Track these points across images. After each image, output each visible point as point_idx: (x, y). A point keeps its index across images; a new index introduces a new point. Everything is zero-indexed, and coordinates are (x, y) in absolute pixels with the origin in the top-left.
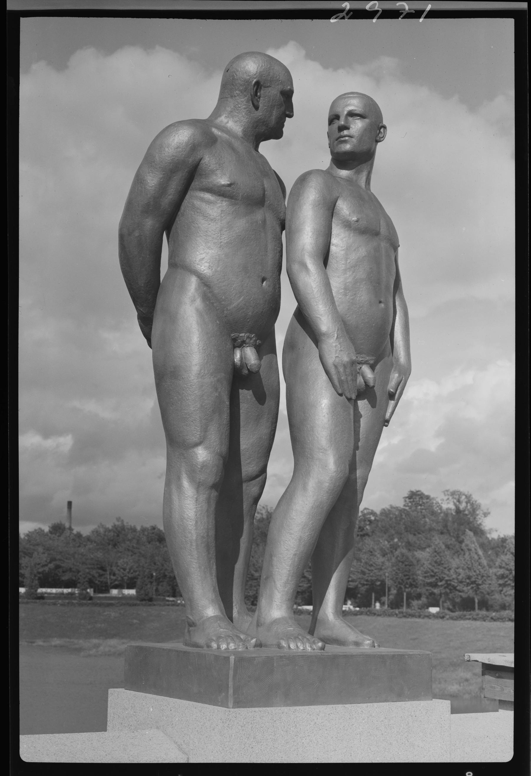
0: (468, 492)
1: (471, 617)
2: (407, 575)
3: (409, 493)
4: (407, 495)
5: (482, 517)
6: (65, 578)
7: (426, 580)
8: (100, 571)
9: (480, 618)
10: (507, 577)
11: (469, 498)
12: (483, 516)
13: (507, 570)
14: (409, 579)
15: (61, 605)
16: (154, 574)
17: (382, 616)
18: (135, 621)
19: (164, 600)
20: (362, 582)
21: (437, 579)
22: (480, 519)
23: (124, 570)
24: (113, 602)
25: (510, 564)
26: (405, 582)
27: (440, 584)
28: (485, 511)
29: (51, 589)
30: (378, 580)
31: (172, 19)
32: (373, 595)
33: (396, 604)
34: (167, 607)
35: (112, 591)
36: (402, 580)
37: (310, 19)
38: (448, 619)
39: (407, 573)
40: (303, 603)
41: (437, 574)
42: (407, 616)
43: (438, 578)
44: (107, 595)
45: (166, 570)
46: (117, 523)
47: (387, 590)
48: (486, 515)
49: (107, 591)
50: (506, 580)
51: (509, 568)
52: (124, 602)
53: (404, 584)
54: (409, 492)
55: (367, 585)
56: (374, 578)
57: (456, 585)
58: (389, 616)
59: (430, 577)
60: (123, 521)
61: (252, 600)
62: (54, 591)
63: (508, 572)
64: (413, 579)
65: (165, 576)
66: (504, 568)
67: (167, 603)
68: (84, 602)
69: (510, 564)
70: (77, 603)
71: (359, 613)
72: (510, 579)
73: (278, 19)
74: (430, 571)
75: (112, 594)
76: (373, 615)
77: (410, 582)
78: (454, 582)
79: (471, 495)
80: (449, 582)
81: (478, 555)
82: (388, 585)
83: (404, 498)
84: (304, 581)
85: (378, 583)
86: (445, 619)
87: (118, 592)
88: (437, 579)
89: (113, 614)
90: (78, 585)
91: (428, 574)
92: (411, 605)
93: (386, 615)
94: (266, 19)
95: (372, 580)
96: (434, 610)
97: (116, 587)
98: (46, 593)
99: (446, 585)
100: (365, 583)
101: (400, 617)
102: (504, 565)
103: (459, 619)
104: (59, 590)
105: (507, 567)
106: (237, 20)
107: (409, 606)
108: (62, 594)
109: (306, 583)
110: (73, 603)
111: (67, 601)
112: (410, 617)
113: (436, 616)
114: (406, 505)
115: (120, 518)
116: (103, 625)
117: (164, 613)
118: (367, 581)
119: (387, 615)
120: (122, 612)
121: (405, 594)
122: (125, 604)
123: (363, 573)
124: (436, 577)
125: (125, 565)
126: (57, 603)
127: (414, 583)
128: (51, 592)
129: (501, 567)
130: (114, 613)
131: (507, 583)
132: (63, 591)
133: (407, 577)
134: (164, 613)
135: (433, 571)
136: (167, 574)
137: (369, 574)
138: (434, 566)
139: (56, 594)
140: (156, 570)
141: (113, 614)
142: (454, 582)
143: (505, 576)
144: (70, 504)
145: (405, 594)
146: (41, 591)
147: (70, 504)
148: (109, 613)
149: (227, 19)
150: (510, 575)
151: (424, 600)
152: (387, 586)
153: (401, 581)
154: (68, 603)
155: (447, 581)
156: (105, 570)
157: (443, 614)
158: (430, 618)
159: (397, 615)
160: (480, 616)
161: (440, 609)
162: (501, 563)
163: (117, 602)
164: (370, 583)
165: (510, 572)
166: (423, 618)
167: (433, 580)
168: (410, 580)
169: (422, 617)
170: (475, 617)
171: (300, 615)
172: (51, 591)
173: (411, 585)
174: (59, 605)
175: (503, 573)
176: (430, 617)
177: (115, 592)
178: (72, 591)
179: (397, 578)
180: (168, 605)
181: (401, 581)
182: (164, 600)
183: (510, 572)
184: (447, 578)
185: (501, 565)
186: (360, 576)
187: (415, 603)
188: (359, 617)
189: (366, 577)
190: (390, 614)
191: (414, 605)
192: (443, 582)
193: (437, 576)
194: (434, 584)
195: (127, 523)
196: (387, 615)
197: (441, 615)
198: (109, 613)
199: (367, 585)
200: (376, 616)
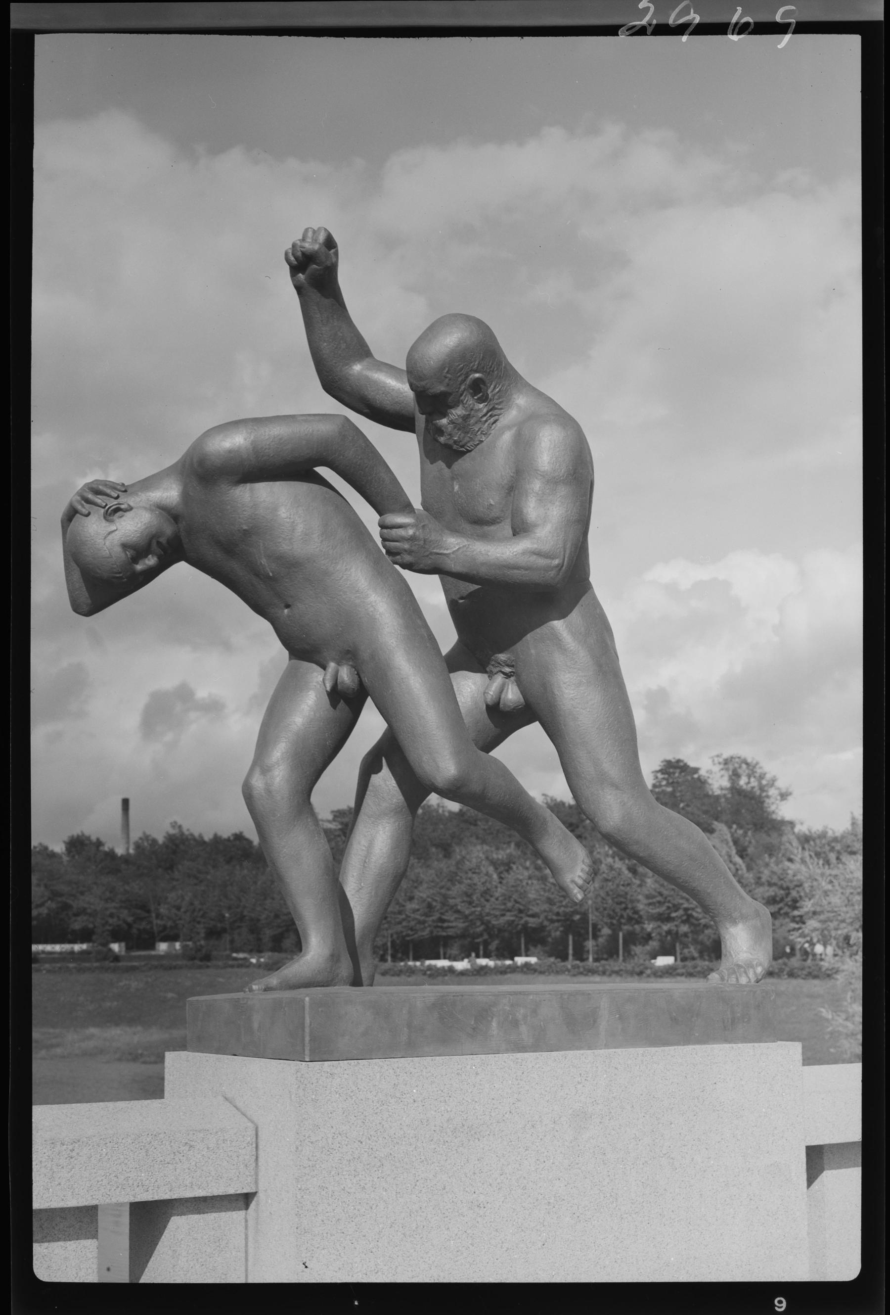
0: (753, 758)
1: (683, 971)
2: (621, 903)
3: (662, 764)
4: (658, 768)
5: (777, 800)
6: (77, 925)
7: (650, 911)
8: (139, 911)
9: (699, 972)
10: (782, 900)
11: (752, 768)
12: (779, 798)
13: (781, 888)
14: (625, 909)
15: (49, 971)
16: (227, 915)
17: (547, 974)
18: (170, 995)
19: (229, 957)
20: (549, 917)
21: (668, 908)
22: (773, 803)
23: (178, 908)
24: (135, 964)
25: (785, 878)
26: (619, 914)
27: (674, 915)
28: (784, 791)
29: (53, 946)
30: (576, 912)
31: (277, 37)
32: (571, 938)
33: (610, 952)
34: (229, 970)
35: (159, 946)
36: (614, 911)
37: (518, 36)
38: (649, 976)
39: (622, 900)
40: (463, 955)
41: (669, 898)
42: (585, 973)
43: (670, 905)
44: (153, 953)
45: (245, 907)
46: (172, 831)
47: (590, 929)
48: (784, 796)
49: (152, 947)
50: (781, 905)
51: (785, 886)
52: (155, 963)
53: (617, 918)
54: (662, 762)
55: (558, 921)
56: (569, 910)
57: (700, 916)
58: (558, 973)
59: (657, 905)
60: (180, 827)
61: (381, 952)
62: (57, 948)
63: (782, 892)
64: (633, 908)
65: (242, 918)
66: (775, 884)
67: (231, 963)
68: (87, 965)
69: (785, 878)
70: (75, 968)
71: (508, 970)
72: (787, 905)
73: (465, 37)
74: (656, 894)
75: (159, 950)
76: (532, 972)
77: (628, 915)
78: (697, 912)
79: (757, 763)
80: (690, 912)
81: (735, 864)
82: (592, 920)
83: (653, 772)
84: (460, 919)
85: (577, 917)
86: (644, 975)
87: (169, 947)
88: (668, 908)
89: (134, 984)
90: (94, 937)
91: (654, 900)
92: (633, 953)
93: (553, 971)
94: (445, 37)
95: (565, 914)
96: (664, 961)
97: (164, 940)
98: (43, 952)
99: (685, 918)
100: (555, 918)
101: (574, 975)
102: (775, 880)
103: (667, 975)
104: (67, 947)
105: (780, 883)
106: (396, 39)
107: (628, 954)
108: (72, 952)
109: (462, 921)
110: (68, 967)
111: (59, 965)
112: (590, 974)
113: (668, 972)
114: (658, 784)
115: (175, 822)
116: (115, 1003)
117: (221, 980)
118: (558, 914)
119: (555, 971)
120: (150, 980)
121: (621, 935)
122: (156, 967)
123: (550, 901)
124: (667, 904)
125: (179, 901)
126: (42, 968)
127: (636, 916)
128: (53, 950)
129: (770, 884)
130: (136, 983)
131: (782, 912)
132: (72, 948)
133: (623, 906)
134: (221, 980)
135: (661, 894)
136: (245, 913)
137: (561, 902)
138: (662, 885)
139: (61, 953)
140: (229, 908)
141: (134, 984)
142: (697, 912)
143: (778, 899)
144: (126, 803)
145: (621, 935)
146: (81, 948)
147: (126, 803)
148: (127, 982)
149: (380, 37)
150: (787, 897)
151: (654, 944)
152: (591, 922)
153: (611, 913)
154: (60, 968)
155: (686, 910)
156: (149, 911)
157: (642, 967)
158: (621, 976)
159: (569, 971)
160: (699, 969)
161: (676, 960)
162: (770, 877)
163: (143, 963)
164: (563, 918)
165: (787, 891)
166: (610, 975)
167: (662, 909)
168: (628, 911)
169: (608, 973)
170: (692, 970)
171: (409, 976)
172: (53, 948)
173: (630, 919)
174: (44, 972)
175: (773, 894)
176: (621, 972)
177: (163, 947)
178: (88, 947)
179: (605, 909)
180: (232, 966)
181: (611, 913)
182: (229, 957)
183: (787, 891)
184: (686, 905)
185: (769, 879)
186: (546, 907)
187: (637, 949)
188: (509, 975)
189: (555, 909)
190: (558, 970)
191: (638, 952)
192: (681, 912)
193: (669, 902)
194: (666, 916)
195: (188, 830)
196: (555, 971)
197: (637, 970)
198: (127, 982)
199: (558, 921)
200: (536, 974)
